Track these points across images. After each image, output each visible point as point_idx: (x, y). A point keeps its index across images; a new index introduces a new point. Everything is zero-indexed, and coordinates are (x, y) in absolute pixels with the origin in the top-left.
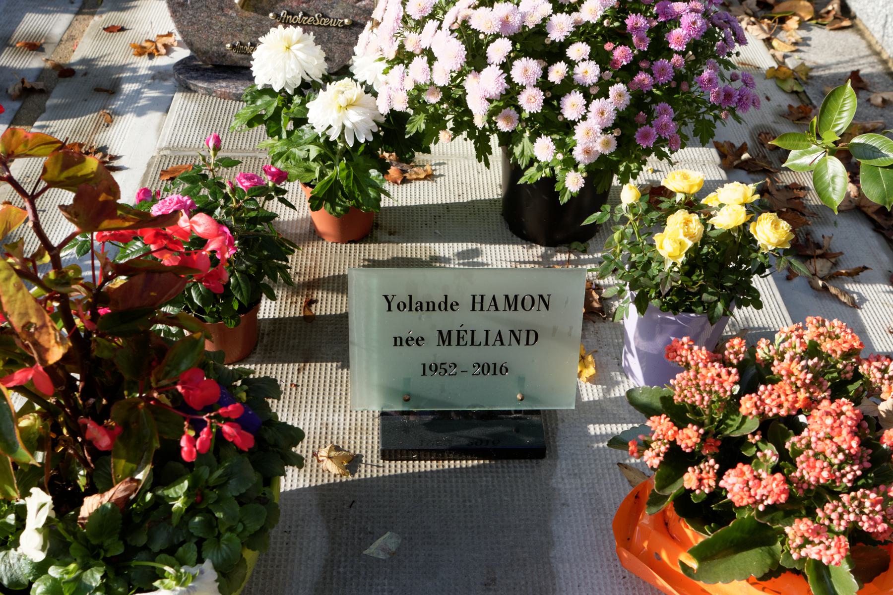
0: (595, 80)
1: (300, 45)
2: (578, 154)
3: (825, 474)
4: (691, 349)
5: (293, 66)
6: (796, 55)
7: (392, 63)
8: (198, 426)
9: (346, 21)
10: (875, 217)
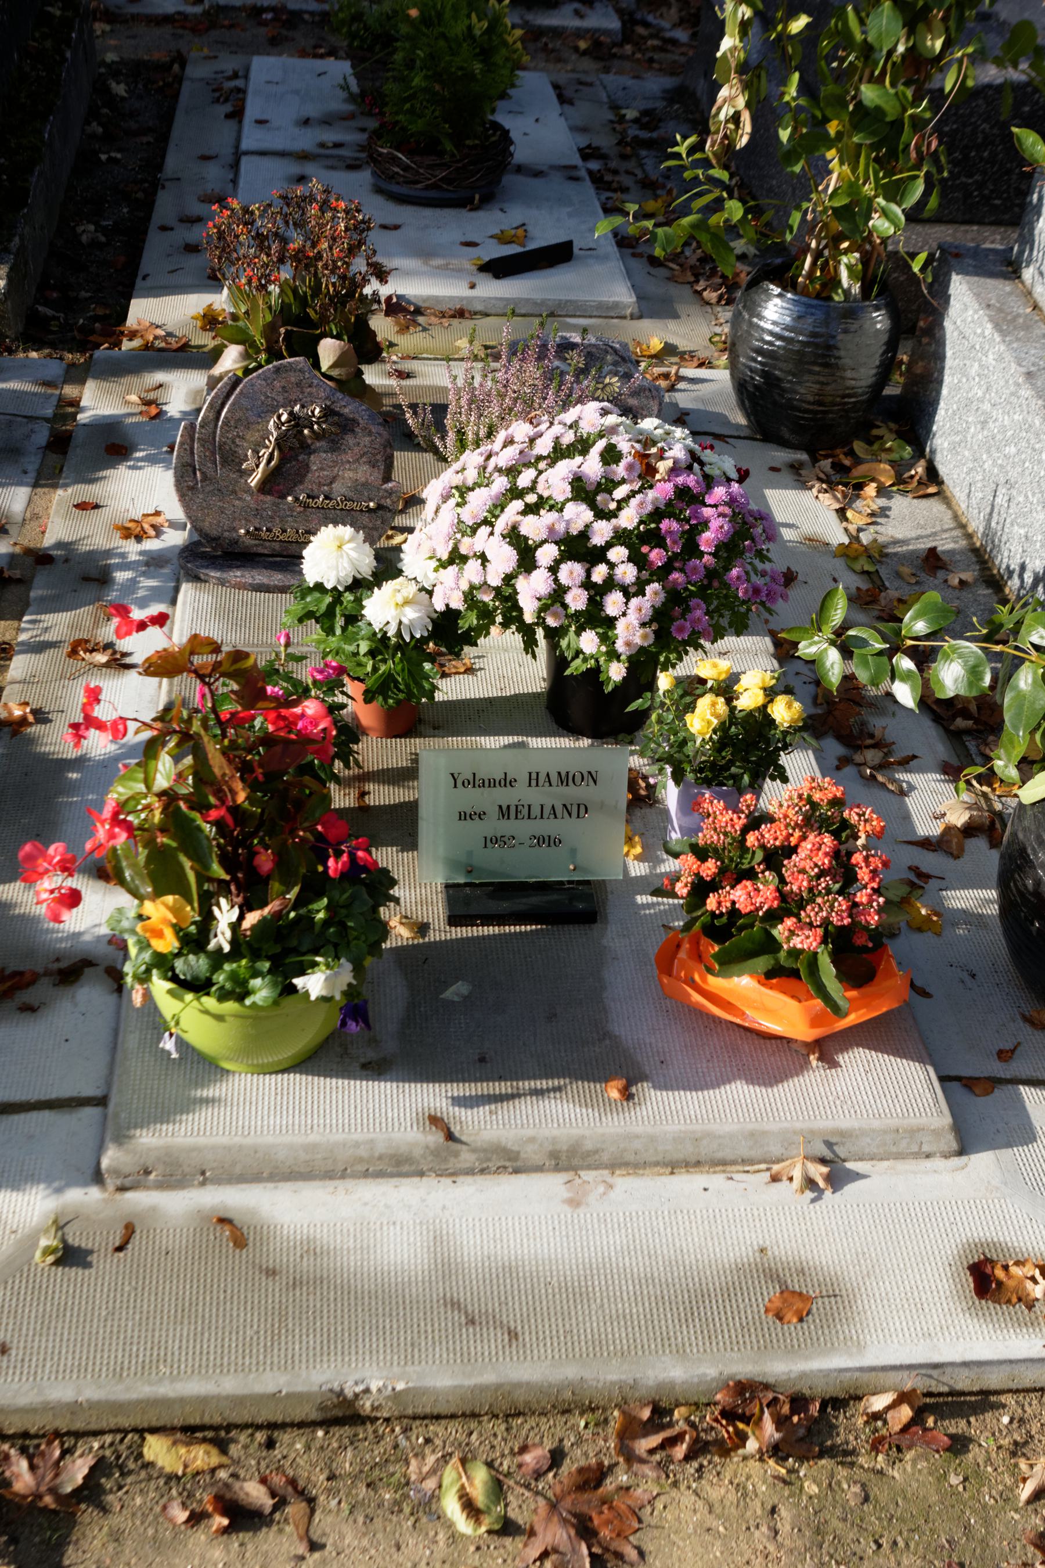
0: (633, 580)
1: (352, 545)
2: (620, 646)
3: (805, 884)
4: (711, 802)
5: (346, 565)
6: (872, 529)
7: (443, 565)
8: (338, 854)
9: (372, 504)
10: (935, 707)
